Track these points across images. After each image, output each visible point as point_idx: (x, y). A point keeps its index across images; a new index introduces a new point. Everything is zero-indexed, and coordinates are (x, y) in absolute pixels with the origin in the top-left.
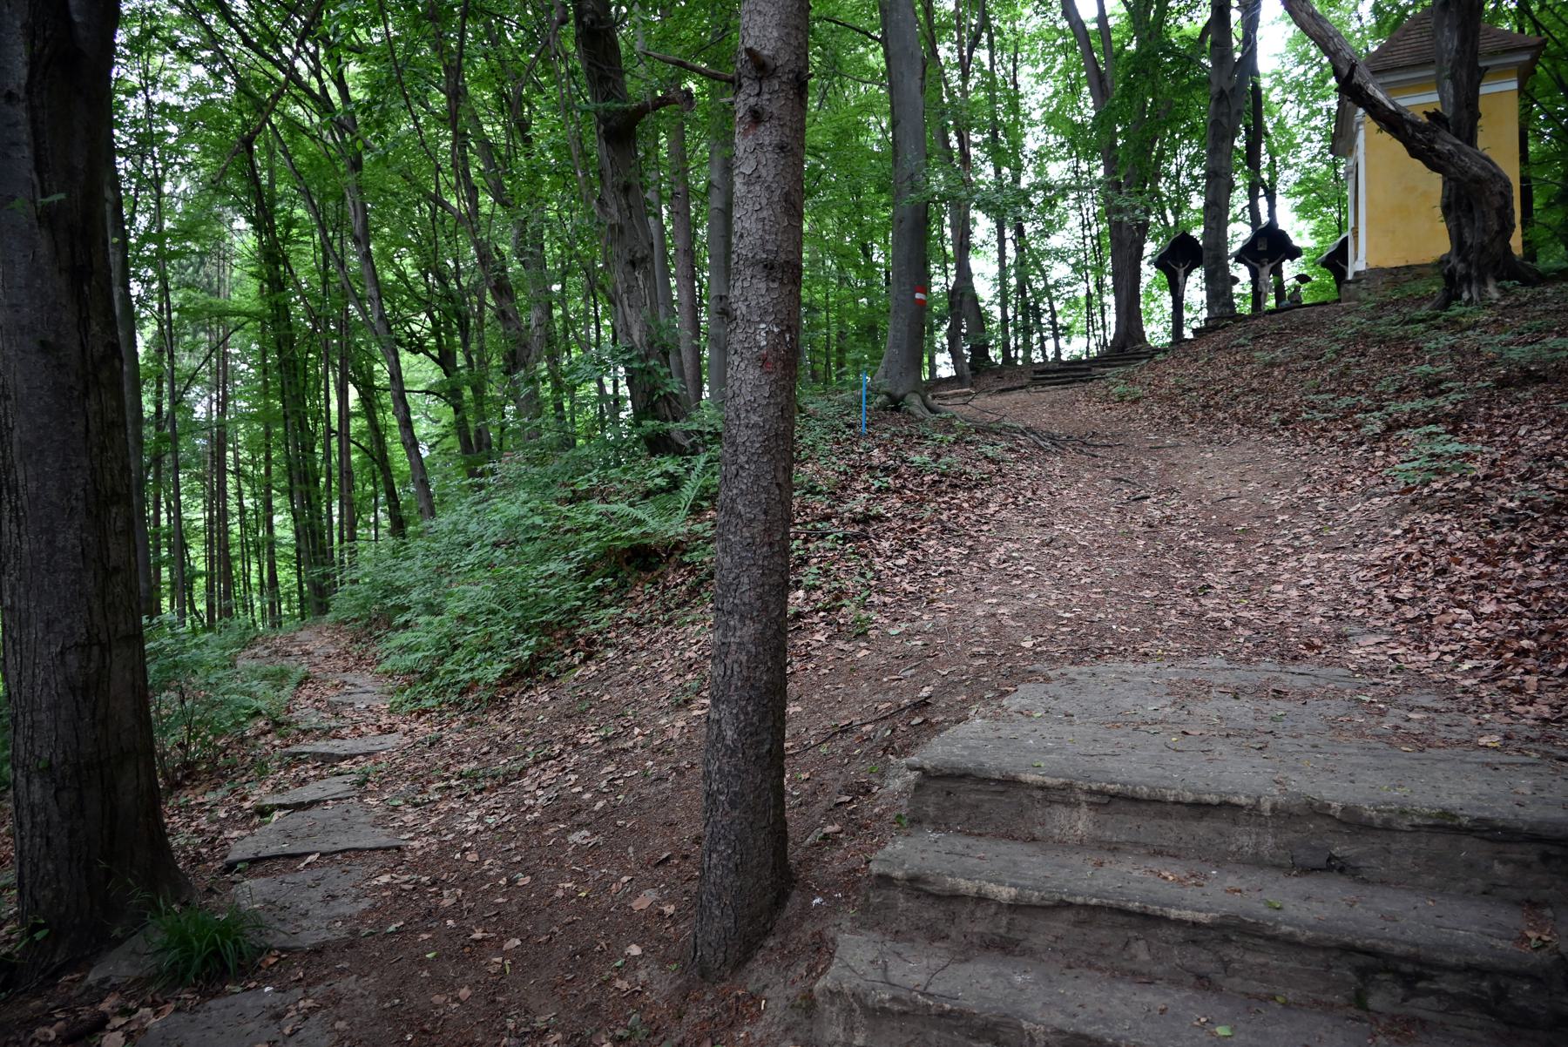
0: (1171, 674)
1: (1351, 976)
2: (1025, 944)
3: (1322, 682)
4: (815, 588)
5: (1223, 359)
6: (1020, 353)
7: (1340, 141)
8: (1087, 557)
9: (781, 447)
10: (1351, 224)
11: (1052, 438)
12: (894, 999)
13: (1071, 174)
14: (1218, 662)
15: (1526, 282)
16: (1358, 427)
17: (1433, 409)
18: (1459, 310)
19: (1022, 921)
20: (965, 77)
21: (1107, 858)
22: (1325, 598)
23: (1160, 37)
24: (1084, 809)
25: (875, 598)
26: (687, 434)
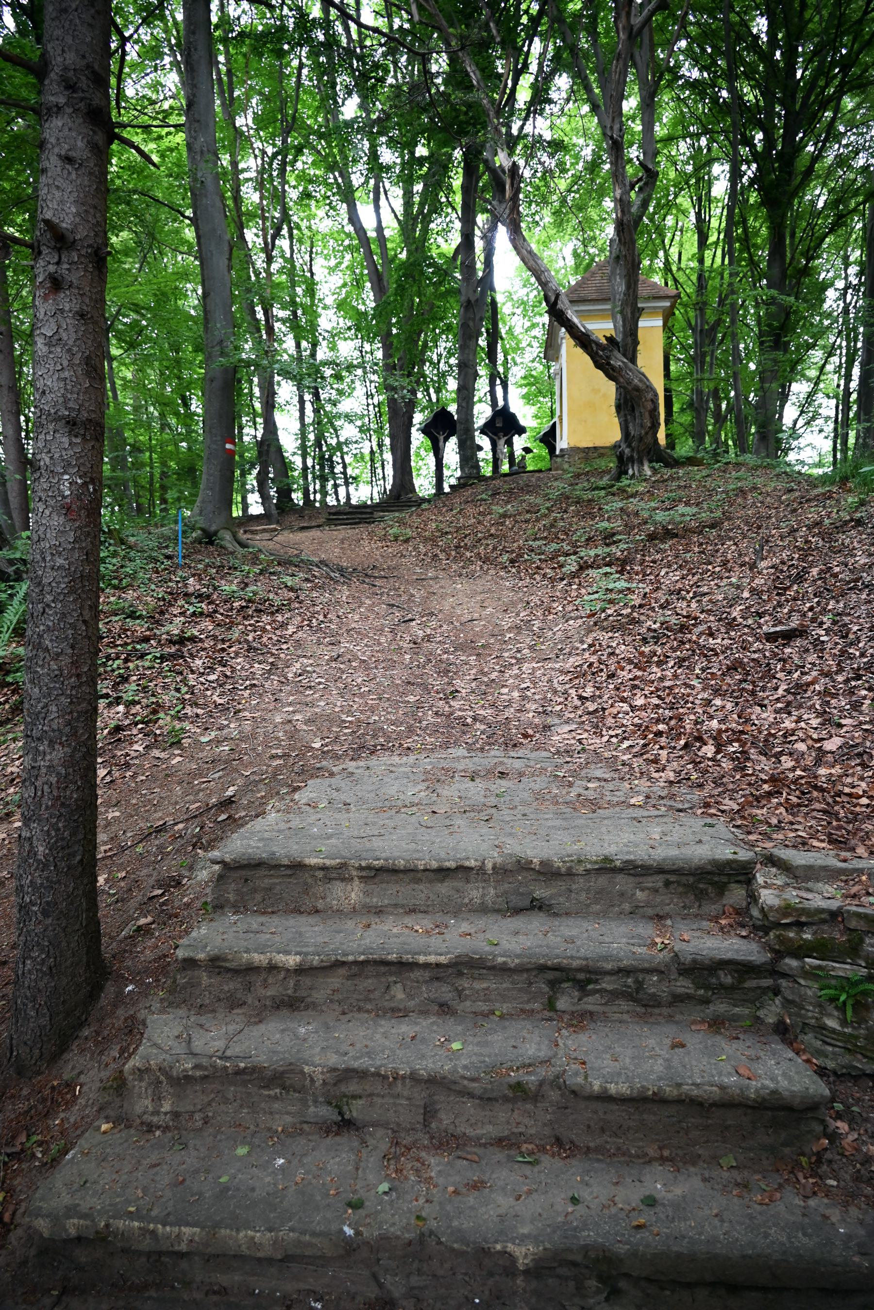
0: (427, 764)
1: (545, 988)
2: (309, 1000)
3: (532, 763)
4: (134, 703)
5: (470, 510)
6: (318, 496)
7: (551, 350)
8: (366, 669)
9: (87, 583)
10: (558, 413)
11: (341, 570)
12: (196, 1067)
13: (357, 354)
14: (461, 752)
15: (667, 465)
16: (561, 566)
17: (609, 555)
18: (627, 482)
19: (307, 981)
20: (269, 260)
21: (374, 919)
22: (537, 697)
23: (424, 252)
24: (356, 882)
25: (189, 710)
26: (11, 562)
